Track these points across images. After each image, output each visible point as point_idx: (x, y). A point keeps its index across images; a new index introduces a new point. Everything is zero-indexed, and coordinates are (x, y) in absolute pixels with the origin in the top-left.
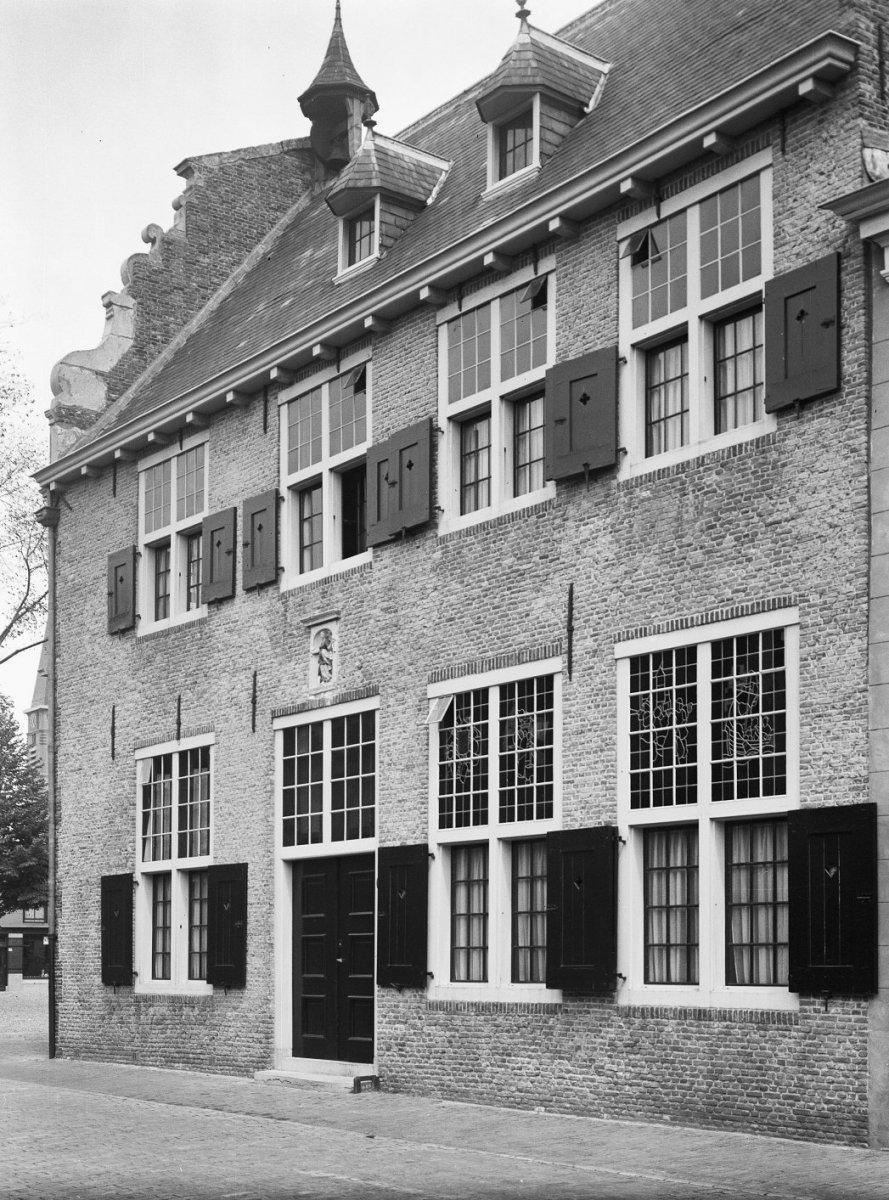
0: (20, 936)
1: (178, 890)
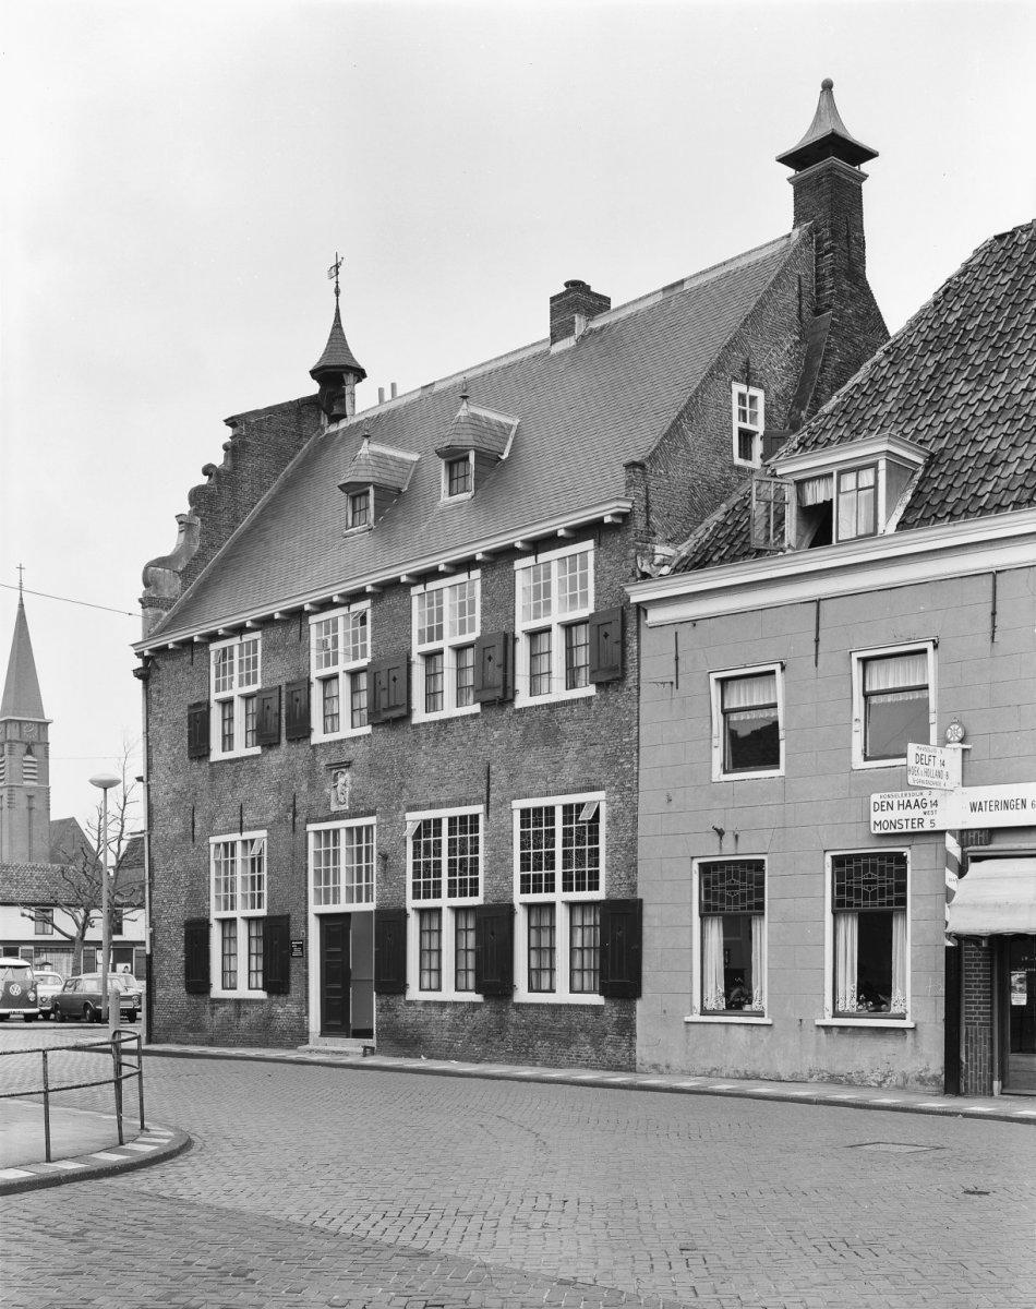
0: (32, 948)
1: (242, 930)
